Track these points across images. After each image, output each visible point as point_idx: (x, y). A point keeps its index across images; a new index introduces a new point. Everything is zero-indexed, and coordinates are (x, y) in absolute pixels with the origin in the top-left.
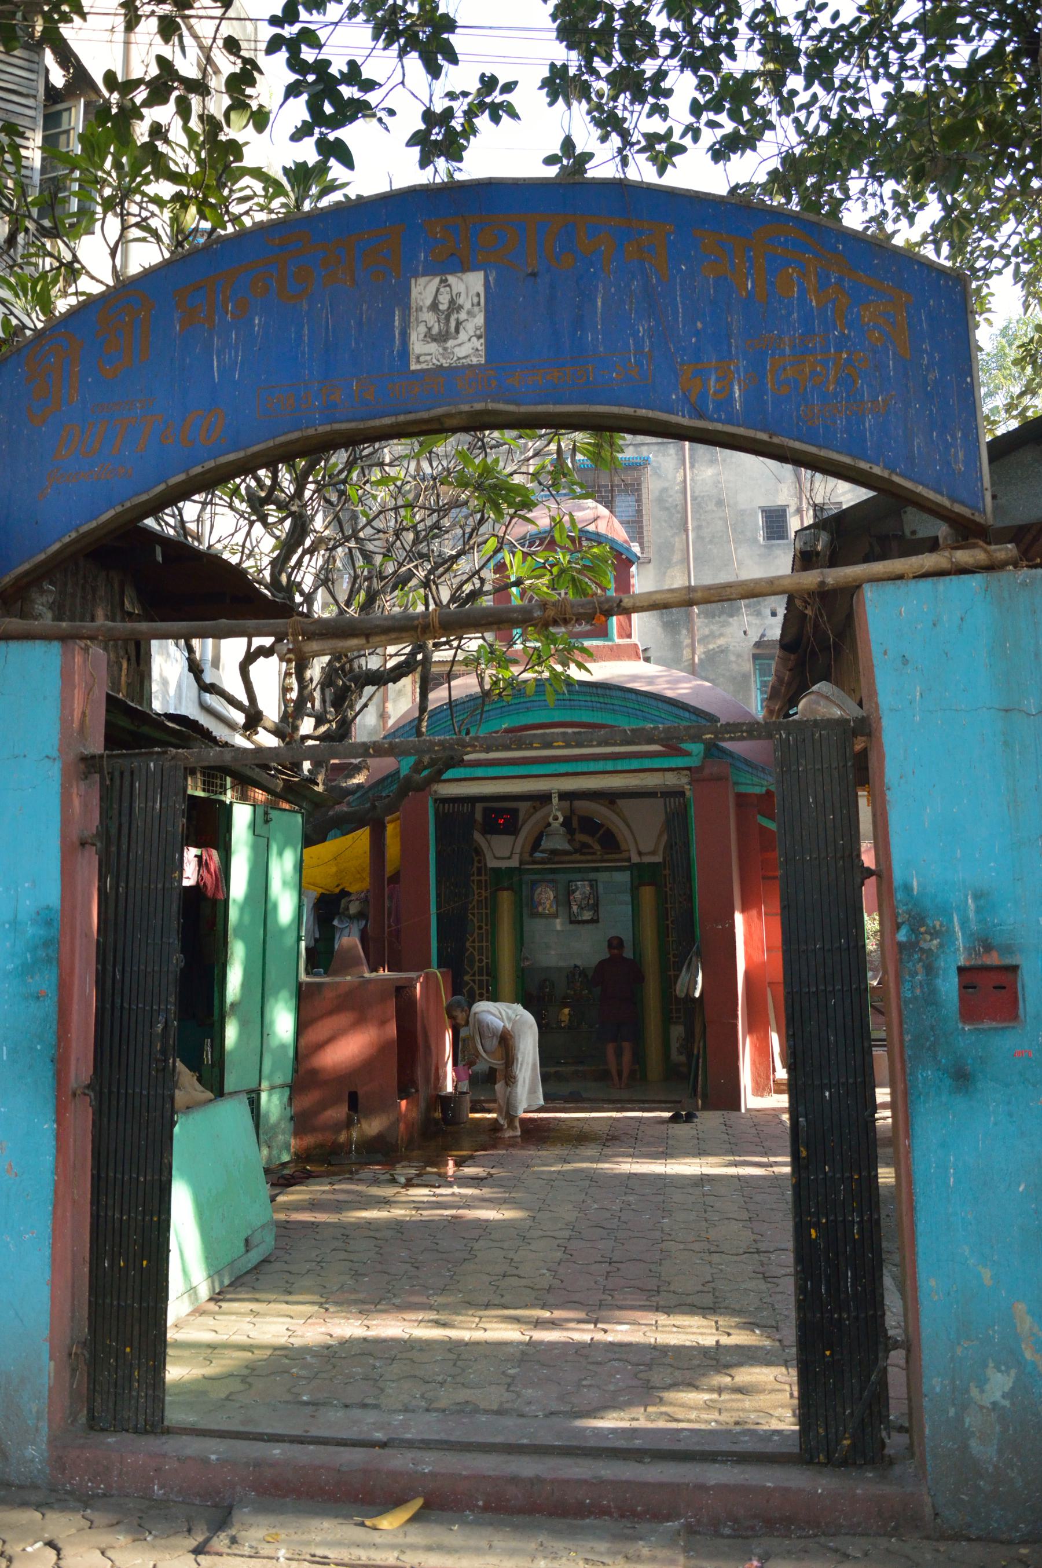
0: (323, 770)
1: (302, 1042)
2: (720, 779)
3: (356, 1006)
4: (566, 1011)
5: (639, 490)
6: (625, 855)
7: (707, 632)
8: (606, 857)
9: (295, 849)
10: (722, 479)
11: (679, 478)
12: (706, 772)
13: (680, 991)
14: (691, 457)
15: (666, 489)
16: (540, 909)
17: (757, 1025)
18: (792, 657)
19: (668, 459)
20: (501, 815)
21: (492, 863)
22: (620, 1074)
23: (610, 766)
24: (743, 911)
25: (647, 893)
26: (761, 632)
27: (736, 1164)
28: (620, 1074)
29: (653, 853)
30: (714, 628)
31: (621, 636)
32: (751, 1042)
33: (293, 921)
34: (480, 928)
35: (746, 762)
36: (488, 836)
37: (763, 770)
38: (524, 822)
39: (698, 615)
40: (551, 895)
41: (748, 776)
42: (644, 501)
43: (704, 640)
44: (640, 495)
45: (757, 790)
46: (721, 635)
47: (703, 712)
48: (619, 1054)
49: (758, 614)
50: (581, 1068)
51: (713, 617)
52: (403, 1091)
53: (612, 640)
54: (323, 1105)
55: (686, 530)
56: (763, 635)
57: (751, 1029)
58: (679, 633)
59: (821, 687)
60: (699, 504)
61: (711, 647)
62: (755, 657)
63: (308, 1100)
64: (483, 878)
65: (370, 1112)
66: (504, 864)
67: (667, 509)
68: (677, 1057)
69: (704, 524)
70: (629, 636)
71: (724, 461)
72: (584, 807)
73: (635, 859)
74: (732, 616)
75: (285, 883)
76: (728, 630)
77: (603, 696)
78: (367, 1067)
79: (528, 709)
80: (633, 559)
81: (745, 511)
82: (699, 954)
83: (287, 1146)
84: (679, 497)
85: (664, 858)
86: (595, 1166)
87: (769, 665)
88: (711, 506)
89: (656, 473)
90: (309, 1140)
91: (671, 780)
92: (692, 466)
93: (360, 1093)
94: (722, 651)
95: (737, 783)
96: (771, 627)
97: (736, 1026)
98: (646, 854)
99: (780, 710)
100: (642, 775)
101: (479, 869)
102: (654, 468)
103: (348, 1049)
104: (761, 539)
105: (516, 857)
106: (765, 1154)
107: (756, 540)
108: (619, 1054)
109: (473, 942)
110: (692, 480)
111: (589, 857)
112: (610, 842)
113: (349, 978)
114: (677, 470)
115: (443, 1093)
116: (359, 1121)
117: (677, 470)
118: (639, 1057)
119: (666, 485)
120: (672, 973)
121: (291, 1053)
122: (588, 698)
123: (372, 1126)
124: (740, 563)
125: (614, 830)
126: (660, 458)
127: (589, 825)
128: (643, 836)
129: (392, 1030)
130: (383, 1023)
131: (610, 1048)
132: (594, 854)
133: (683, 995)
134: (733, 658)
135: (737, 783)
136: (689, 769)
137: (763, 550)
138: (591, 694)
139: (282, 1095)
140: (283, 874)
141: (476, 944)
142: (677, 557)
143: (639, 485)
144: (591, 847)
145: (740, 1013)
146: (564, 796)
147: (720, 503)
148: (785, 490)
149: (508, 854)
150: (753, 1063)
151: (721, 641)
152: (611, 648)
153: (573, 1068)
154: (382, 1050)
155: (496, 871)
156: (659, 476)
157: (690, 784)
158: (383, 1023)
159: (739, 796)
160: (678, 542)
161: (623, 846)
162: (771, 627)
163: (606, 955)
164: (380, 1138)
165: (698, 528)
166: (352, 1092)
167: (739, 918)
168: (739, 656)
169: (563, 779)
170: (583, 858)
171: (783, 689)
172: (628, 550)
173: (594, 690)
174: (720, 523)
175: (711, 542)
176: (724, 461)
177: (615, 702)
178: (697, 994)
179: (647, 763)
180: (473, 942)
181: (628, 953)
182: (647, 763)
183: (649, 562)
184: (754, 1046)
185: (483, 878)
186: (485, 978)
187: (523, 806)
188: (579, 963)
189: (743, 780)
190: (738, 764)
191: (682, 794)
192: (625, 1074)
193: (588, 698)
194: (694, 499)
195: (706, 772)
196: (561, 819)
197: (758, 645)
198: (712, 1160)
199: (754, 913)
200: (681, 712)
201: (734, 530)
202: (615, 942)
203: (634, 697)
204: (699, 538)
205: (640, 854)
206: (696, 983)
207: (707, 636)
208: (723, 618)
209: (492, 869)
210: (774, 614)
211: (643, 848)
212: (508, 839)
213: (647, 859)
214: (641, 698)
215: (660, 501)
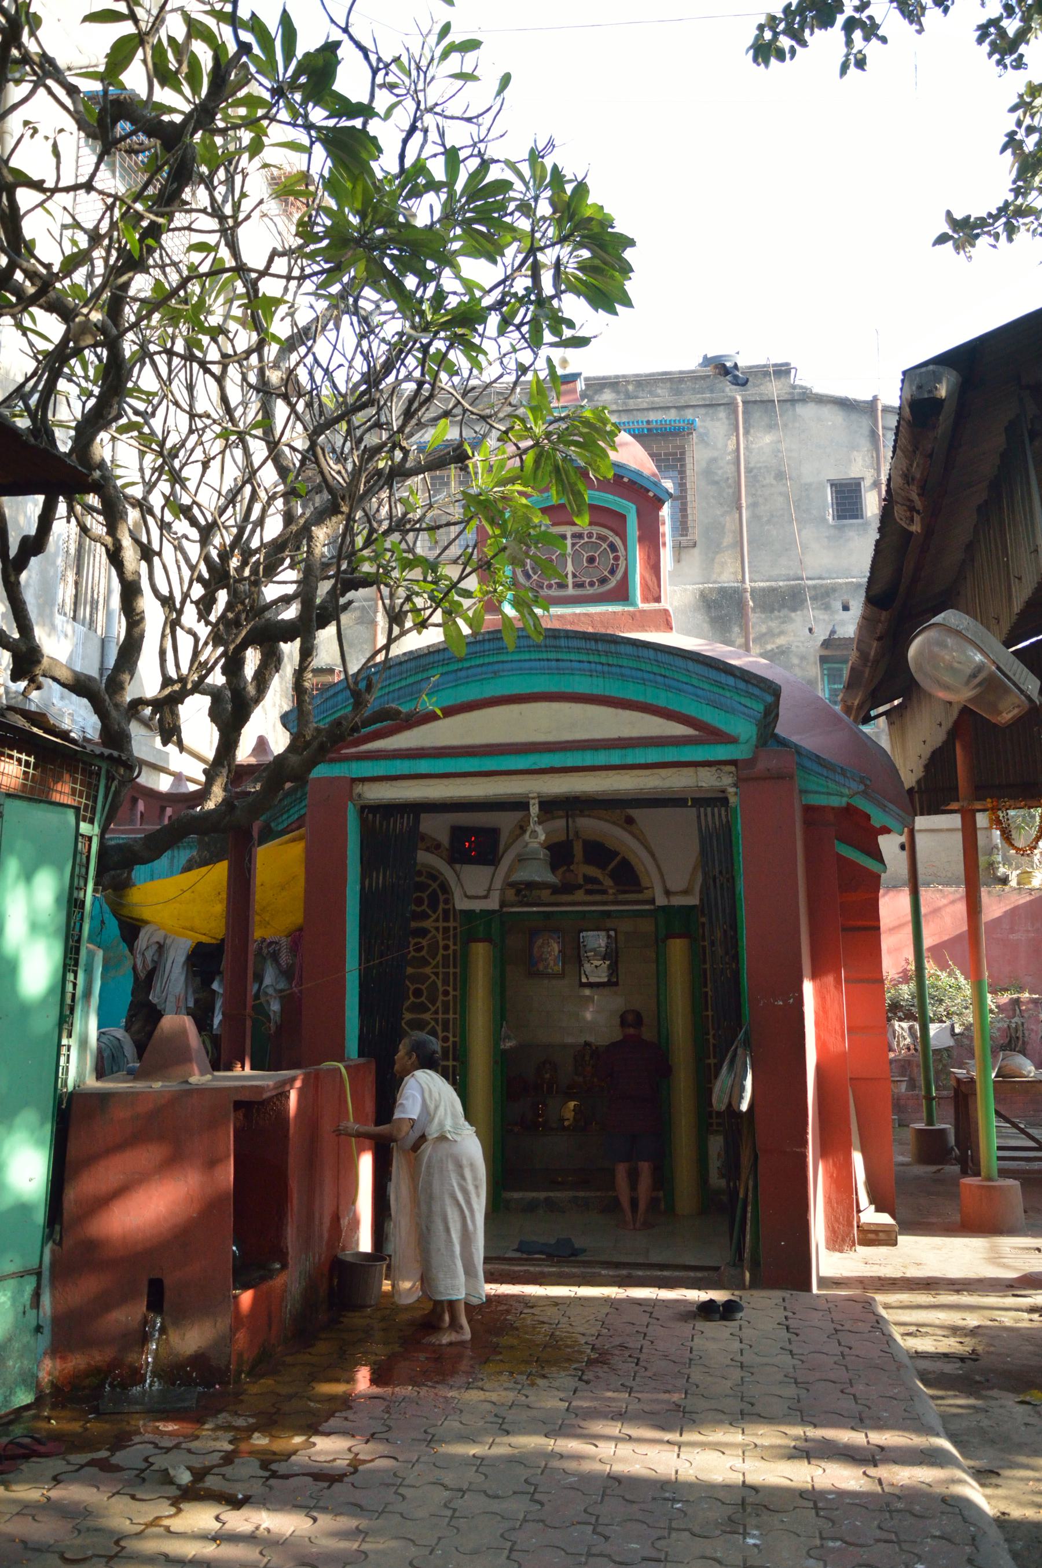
0: (225, 772)
1: (71, 1195)
2: (782, 777)
3: (167, 1133)
4: (572, 1104)
5: (682, 459)
6: (646, 895)
7: (764, 629)
8: (621, 897)
9: (61, 870)
10: (783, 446)
11: (731, 446)
12: (761, 765)
13: (719, 1102)
14: (745, 422)
15: (714, 460)
16: (541, 967)
17: (834, 1147)
18: (884, 615)
19: (718, 424)
20: (477, 837)
21: (462, 904)
22: (634, 1203)
23: (615, 757)
24: (814, 977)
25: (678, 949)
26: (830, 628)
27: (806, 1452)
28: (634, 1203)
29: (686, 892)
30: (773, 624)
31: (646, 600)
32: (825, 1171)
33: (51, 991)
34: (446, 993)
35: (818, 759)
36: (457, 867)
37: (843, 773)
38: (507, 848)
39: (754, 609)
40: (556, 948)
41: (822, 781)
42: (688, 473)
43: (761, 639)
44: (683, 466)
45: (836, 802)
46: (782, 633)
47: (756, 676)
48: (633, 1177)
49: (827, 607)
50: (582, 1194)
51: (772, 611)
52: (247, 1272)
53: (634, 604)
54: (104, 1303)
55: (739, 508)
56: (833, 632)
57: (825, 1150)
58: (730, 631)
59: (948, 617)
60: (755, 477)
61: (769, 647)
62: (823, 660)
63: (86, 1288)
64: (451, 924)
65: (181, 1316)
66: (477, 906)
67: (716, 483)
68: (716, 1181)
69: (761, 500)
70: (658, 600)
71: (785, 425)
72: (590, 826)
73: (661, 901)
74: (794, 610)
75: (35, 927)
76: (789, 627)
77: (607, 653)
78: (181, 1239)
79: (496, 674)
80: (663, 496)
81: (810, 485)
82: (747, 1043)
83: (28, 1379)
84: (731, 468)
85: (701, 900)
86: (550, 1444)
87: (841, 670)
88: (770, 479)
89: (703, 440)
90: (78, 1362)
91: (707, 780)
92: (747, 432)
93: (167, 1282)
94: (783, 653)
95: (804, 792)
96: (843, 623)
97: (805, 1156)
98: (676, 893)
99: (860, 707)
100: (663, 772)
101: (446, 912)
102: (700, 435)
103: (150, 1206)
104: (830, 518)
105: (496, 896)
106: (860, 1422)
107: (824, 520)
108: (633, 1177)
109: (436, 1012)
110: (746, 448)
111: (598, 898)
112: (627, 876)
113: (157, 1085)
114: (728, 437)
115: (347, 1256)
116: (163, 1330)
117: (728, 437)
118: (663, 1179)
119: (716, 454)
120: (712, 1061)
121: (40, 1216)
122: (584, 658)
123: (191, 1339)
124: (805, 548)
125: (634, 861)
126: (709, 424)
127: (599, 853)
128: (671, 870)
129: (227, 1174)
130: (212, 1163)
131: (621, 1171)
132: (604, 892)
133: (723, 1107)
134: (795, 661)
135: (804, 792)
136: (733, 763)
137: (832, 532)
138: (588, 651)
139: (20, 1291)
140: (32, 910)
141: (440, 1016)
142: (728, 540)
143: (683, 453)
144: (600, 883)
145: (810, 1137)
146: (550, 806)
147: (780, 476)
148: (860, 461)
149: (482, 892)
150: (828, 1201)
151: (781, 641)
152: (632, 616)
153: (571, 1194)
154: (209, 1209)
155: (468, 914)
156: (707, 444)
157: (735, 785)
158: (212, 1163)
159: (808, 809)
160: (729, 522)
161: (645, 882)
162: (843, 623)
163: (617, 1035)
164: (199, 1360)
165: (753, 505)
166: (155, 1279)
167: (808, 988)
168: (803, 658)
169: (546, 777)
170: (589, 898)
171: (867, 670)
172: (657, 484)
173: (592, 645)
174: (781, 499)
175: (769, 522)
176: (785, 425)
177: (625, 662)
178: (744, 1107)
179: (671, 754)
180: (436, 1012)
181: (648, 1034)
182: (671, 754)
183: (695, 546)
184: (828, 1175)
185: (451, 924)
186: (450, 1063)
187: (506, 821)
188: (591, 1039)
189: (813, 787)
190: (808, 764)
191: (724, 801)
192: (642, 1206)
193: (584, 658)
194: (749, 471)
195: (761, 765)
196: (542, 837)
197: (826, 644)
198: (767, 1436)
199: (830, 979)
200: (723, 678)
201: (797, 507)
202: (630, 1018)
203: (651, 654)
204: (755, 518)
205: (668, 893)
206: (742, 1088)
207: (764, 635)
208: (785, 612)
209: (464, 912)
210: (846, 608)
211: (673, 887)
212: (486, 871)
213: (677, 901)
214: (661, 657)
215: (708, 472)
